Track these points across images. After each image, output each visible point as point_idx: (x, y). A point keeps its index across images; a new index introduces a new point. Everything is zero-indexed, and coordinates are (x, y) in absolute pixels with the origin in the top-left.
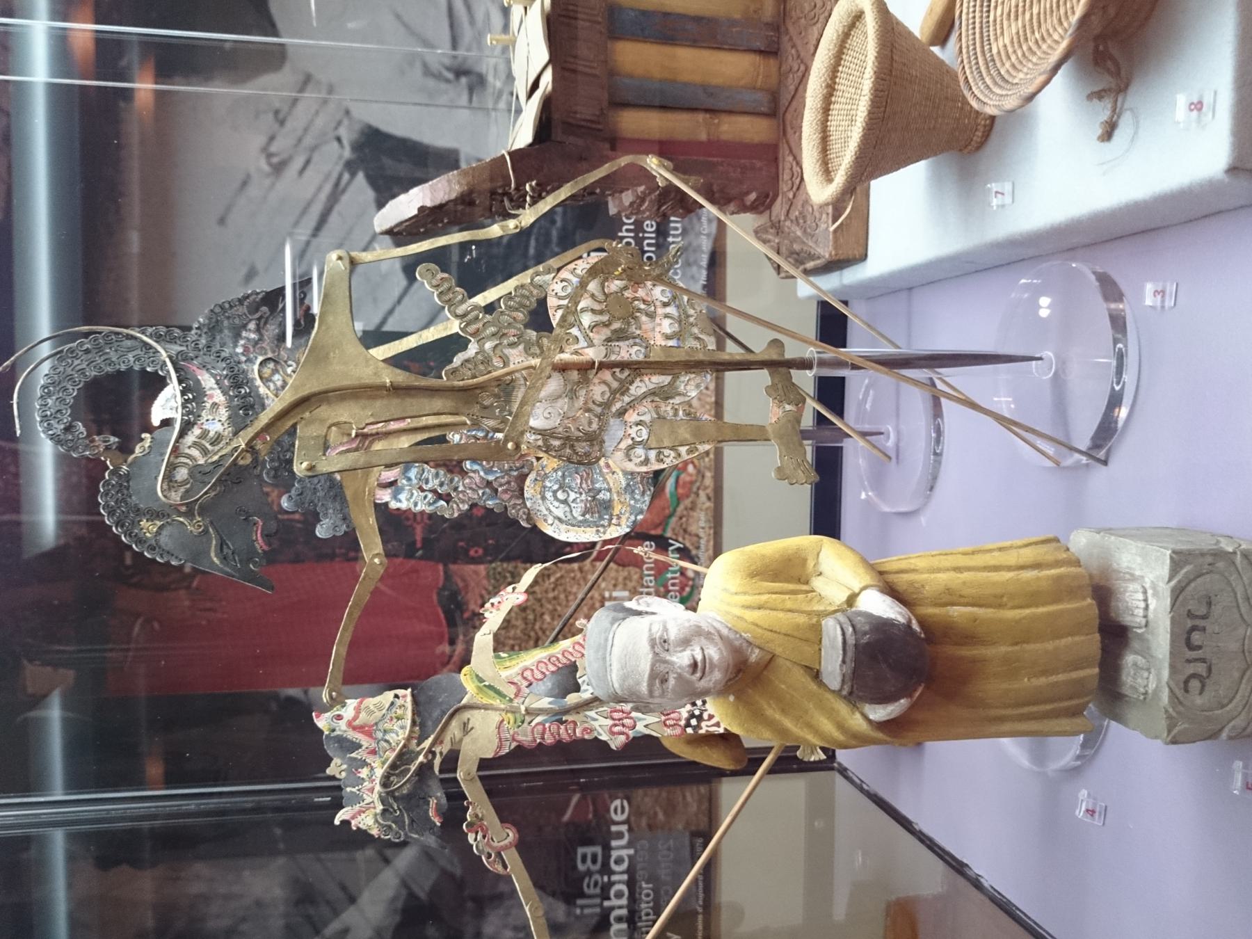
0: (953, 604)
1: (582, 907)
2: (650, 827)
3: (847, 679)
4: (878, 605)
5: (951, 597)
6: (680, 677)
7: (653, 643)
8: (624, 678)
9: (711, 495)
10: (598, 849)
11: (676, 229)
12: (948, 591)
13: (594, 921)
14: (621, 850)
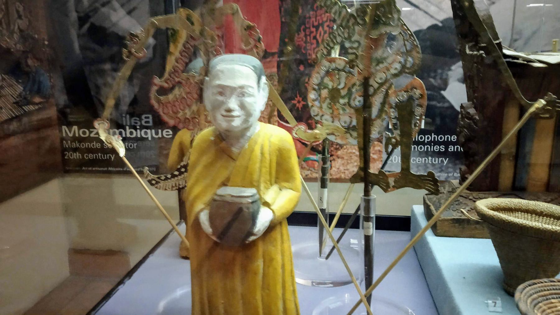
0: (264, 262)
1: (125, 117)
2: (161, 147)
3: (223, 198)
4: (264, 218)
5: (269, 261)
6: (223, 103)
7: (242, 87)
8: (222, 72)
9: (308, 177)
10: (151, 124)
11: (435, 161)
12: (272, 260)
13: (120, 122)
14: (150, 134)
